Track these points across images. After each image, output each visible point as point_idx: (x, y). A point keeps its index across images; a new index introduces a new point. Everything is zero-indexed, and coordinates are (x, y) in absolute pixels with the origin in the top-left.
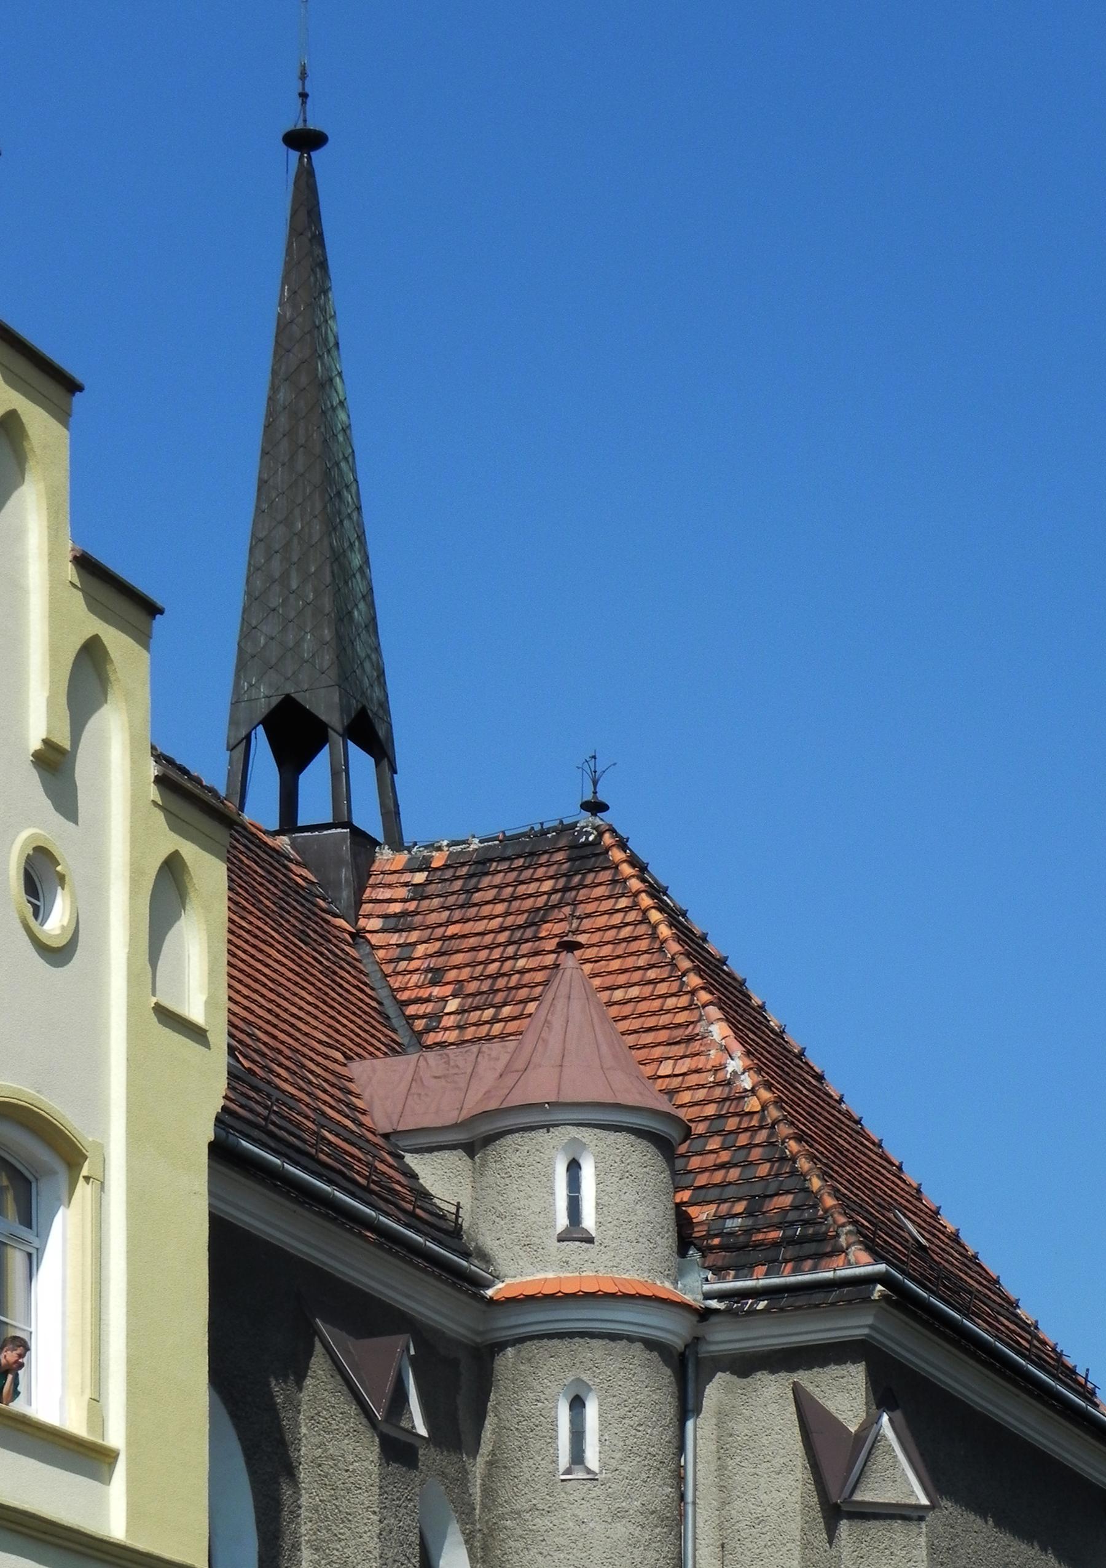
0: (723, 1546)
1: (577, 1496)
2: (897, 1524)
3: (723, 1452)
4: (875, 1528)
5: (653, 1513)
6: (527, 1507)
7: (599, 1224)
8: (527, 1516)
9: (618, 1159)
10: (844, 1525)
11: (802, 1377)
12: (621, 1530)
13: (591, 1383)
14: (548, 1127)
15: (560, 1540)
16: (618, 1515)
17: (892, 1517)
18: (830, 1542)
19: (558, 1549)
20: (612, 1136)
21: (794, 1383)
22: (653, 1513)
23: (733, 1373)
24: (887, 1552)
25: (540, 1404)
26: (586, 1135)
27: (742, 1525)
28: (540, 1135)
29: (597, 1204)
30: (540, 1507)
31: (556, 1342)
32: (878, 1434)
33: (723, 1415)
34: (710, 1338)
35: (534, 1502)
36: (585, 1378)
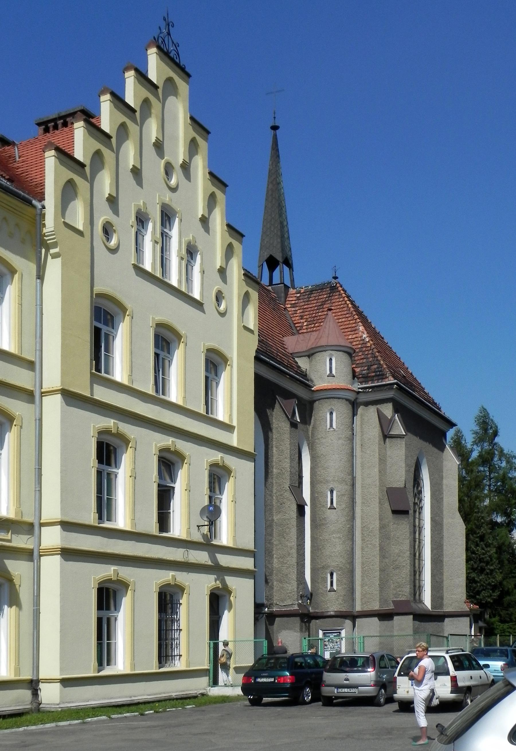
7: (336, 373)
8: (321, 439)
10: (387, 439)
11: (379, 406)
12: (340, 442)
14: (325, 351)
16: (339, 439)
17: (398, 437)
18: (384, 443)
20: (339, 352)
26: (333, 352)
28: (324, 353)
33: (362, 415)
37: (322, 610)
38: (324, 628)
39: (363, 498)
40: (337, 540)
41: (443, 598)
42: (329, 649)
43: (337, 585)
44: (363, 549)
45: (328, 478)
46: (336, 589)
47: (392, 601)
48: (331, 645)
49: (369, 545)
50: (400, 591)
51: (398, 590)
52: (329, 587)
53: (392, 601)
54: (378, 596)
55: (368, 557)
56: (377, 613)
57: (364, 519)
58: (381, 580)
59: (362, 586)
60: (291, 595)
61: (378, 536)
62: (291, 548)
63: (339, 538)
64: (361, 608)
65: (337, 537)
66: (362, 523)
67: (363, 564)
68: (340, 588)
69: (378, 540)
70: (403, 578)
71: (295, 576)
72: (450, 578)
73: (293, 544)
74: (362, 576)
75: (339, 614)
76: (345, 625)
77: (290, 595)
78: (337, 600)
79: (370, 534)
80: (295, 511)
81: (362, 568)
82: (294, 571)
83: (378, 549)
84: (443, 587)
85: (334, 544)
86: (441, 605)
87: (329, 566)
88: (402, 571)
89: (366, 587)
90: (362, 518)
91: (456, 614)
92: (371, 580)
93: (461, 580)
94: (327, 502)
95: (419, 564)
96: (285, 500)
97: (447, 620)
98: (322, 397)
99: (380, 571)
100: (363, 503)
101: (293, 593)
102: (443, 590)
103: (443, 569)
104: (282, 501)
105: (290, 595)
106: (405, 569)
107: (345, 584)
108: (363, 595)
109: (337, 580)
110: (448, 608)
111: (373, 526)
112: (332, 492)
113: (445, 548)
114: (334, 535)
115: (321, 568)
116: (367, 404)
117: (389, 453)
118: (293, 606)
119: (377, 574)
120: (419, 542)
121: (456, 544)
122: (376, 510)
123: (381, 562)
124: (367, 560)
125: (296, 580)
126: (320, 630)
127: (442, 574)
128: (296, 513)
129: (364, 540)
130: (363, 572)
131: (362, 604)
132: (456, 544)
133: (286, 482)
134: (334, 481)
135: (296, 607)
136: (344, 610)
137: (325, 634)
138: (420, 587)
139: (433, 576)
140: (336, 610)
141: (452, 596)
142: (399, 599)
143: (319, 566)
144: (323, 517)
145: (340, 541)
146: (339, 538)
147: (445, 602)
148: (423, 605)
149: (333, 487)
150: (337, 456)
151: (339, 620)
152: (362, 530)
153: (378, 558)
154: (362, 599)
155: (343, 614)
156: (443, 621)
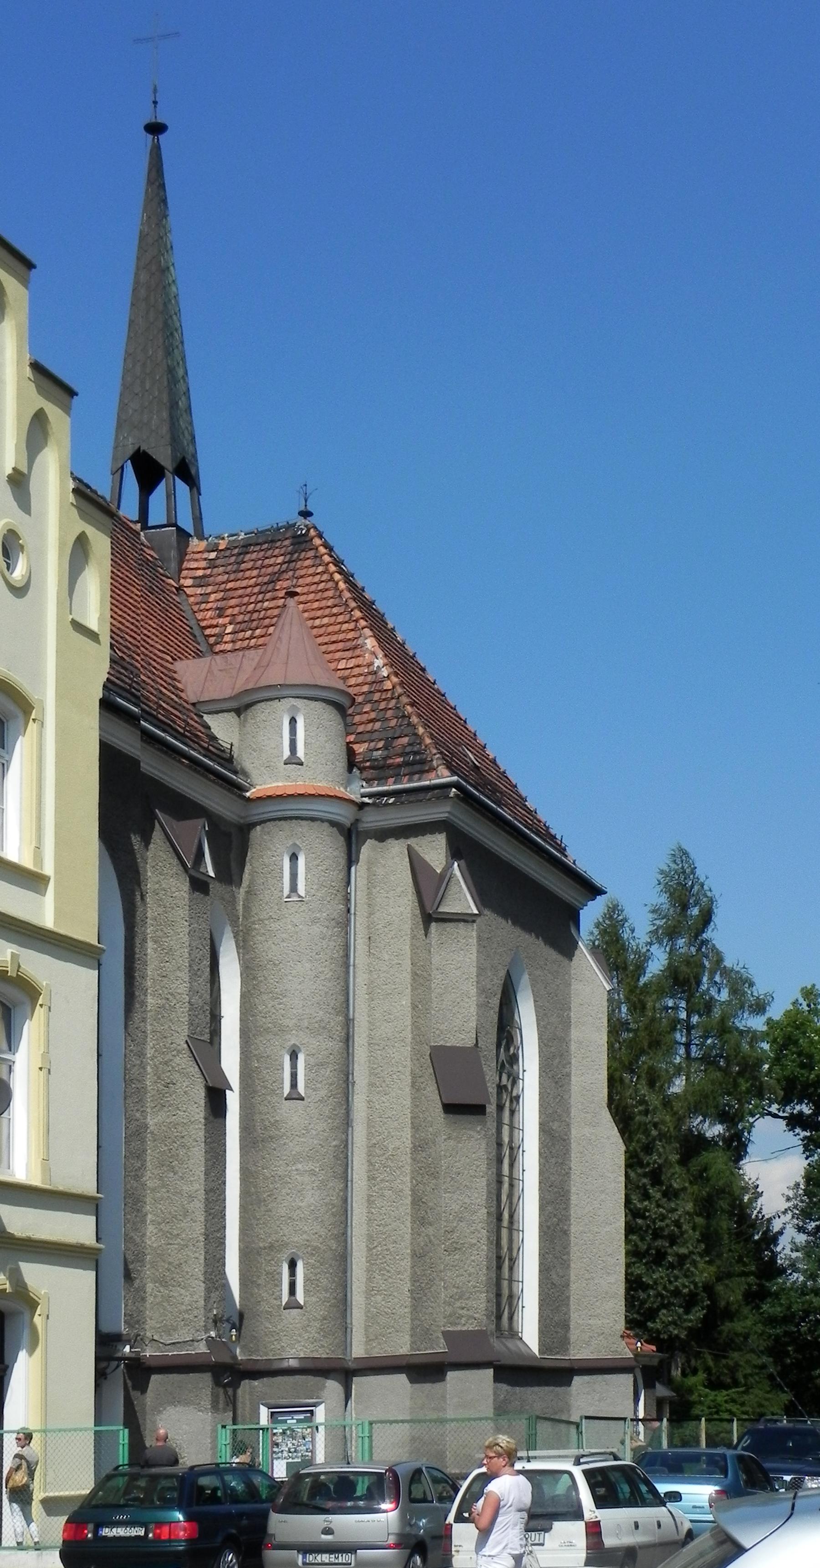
0: (370, 938)
1: (293, 910)
2: (461, 925)
3: (371, 884)
4: (449, 926)
5: (333, 919)
6: (267, 917)
7: (306, 754)
8: (266, 922)
9: (316, 717)
10: (433, 925)
11: (412, 841)
13: (301, 846)
15: (284, 935)
16: (315, 921)
18: (426, 936)
19: (283, 941)
20: (313, 704)
21: (408, 845)
22: (333, 919)
23: (376, 840)
24: (456, 940)
25: (274, 858)
26: (299, 703)
27: (380, 926)
28: (276, 703)
29: (305, 743)
30: (273, 917)
31: (282, 822)
32: (452, 874)
33: (370, 864)
34: (363, 820)
35: (271, 914)
36: (298, 843)
37: (267, 1354)
38: (272, 1402)
39: (372, 1073)
40: (306, 1179)
41: (568, 1326)
42: (285, 1454)
43: (306, 1292)
44: (370, 1201)
45: (286, 1022)
46: (302, 1303)
47: (443, 1333)
48: (290, 1445)
49: (388, 1193)
50: (463, 1308)
51: (458, 1304)
52: (285, 1297)
53: (443, 1333)
54: (408, 1320)
55: (383, 1222)
56: (404, 1363)
57: (373, 1127)
58: (415, 1279)
59: (369, 1293)
60: (191, 1317)
61: (408, 1169)
62: (191, 1198)
63: (312, 1173)
64: (367, 1351)
65: (306, 1171)
66: (370, 1135)
67: (370, 1238)
68: (314, 1299)
69: (408, 1178)
70: (470, 1275)
71: (201, 1268)
72: (587, 1276)
73: (196, 1186)
74: (368, 1270)
75: (309, 1365)
76: (325, 1393)
77: (186, 1316)
78: (305, 1328)
79: (390, 1163)
80: (202, 1102)
81: (370, 1250)
82: (197, 1255)
83: (408, 1201)
84: (568, 1298)
85: (299, 1188)
86: (564, 1344)
87: (286, 1245)
88: (467, 1259)
89: (379, 1298)
90: (370, 1123)
91: (599, 1365)
92: (390, 1280)
93: (613, 1281)
94: (283, 1083)
95: (511, 1240)
96: (177, 1076)
97: (577, 1380)
98: (272, 814)
99: (412, 1257)
100: (371, 1085)
101: (195, 1313)
102: (568, 1305)
103: (568, 1253)
104: (168, 1077)
105: (186, 1316)
106: (475, 1252)
107: (326, 1291)
108: (371, 1318)
109: (307, 1280)
110: (579, 1352)
111: (398, 1143)
112: (294, 1056)
113: (574, 1199)
114: (300, 1166)
115: (265, 1248)
116: (383, 835)
117: (436, 959)
118: (196, 1344)
119: (407, 1263)
120: (511, 1186)
121: (603, 1192)
122: (405, 1102)
123: (415, 1234)
124: (381, 1228)
125: (202, 1279)
126: (262, 1407)
127: (566, 1265)
128: (203, 1109)
129: (374, 1178)
130: (371, 1260)
131: (368, 1341)
132: (603, 1192)
133: (179, 1030)
134: (298, 1027)
135: (202, 1348)
136: (324, 1356)
137: (276, 1415)
138: (511, 1296)
139: (545, 1270)
140: (302, 1355)
141: (590, 1322)
142: (459, 1328)
143: (261, 1245)
144: (272, 1120)
145: (313, 1182)
146: (312, 1173)
147: (574, 1335)
148: (519, 1343)
149: (298, 1044)
150: (308, 966)
151: (311, 1380)
152: (369, 1154)
153: (409, 1225)
154: (367, 1328)
155: (319, 1365)
156: (569, 1383)
